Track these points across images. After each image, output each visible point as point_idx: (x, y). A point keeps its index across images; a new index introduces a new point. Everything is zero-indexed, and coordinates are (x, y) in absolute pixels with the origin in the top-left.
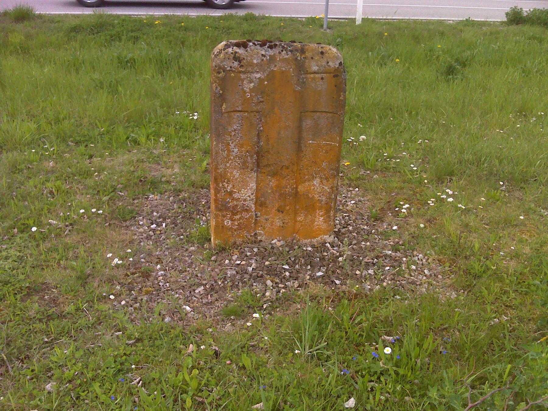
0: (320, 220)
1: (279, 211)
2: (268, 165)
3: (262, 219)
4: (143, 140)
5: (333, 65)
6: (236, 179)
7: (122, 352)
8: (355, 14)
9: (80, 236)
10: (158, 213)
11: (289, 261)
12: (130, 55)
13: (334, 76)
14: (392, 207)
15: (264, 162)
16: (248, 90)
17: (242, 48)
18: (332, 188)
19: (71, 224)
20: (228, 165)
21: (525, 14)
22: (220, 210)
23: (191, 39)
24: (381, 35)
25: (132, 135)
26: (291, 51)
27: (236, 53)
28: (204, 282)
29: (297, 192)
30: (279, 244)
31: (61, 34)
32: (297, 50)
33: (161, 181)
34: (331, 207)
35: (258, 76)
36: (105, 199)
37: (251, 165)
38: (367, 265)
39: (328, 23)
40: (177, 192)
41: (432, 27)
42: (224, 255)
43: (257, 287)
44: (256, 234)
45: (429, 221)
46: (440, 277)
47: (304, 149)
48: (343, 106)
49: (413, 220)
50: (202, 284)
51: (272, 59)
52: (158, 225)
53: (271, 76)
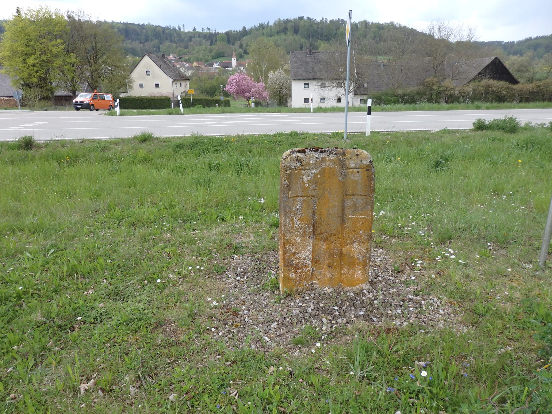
0: (358, 273)
1: (329, 266)
2: (321, 233)
3: (317, 273)
5: (366, 162)
8: (366, 129)
10: (241, 268)
11: (338, 303)
13: (366, 170)
15: (318, 231)
16: (306, 182)
18: (367, 249)
19: (183, 277)
20: (293, 234)
21: (487, 123)
22: (287, 266)
23: (255, 149)
26: (336, 154)
27: (298, 157)
29: (342, 253)
30: (329, 291)
31: (171, 150)
34: (366, 264)
35: (314, 171)
37: (308, 234)
40: (253, 254)
42: (290, 299)
44: (312, 284)
46: (452, 315)
47: (346, 221)
53: (322, 172)
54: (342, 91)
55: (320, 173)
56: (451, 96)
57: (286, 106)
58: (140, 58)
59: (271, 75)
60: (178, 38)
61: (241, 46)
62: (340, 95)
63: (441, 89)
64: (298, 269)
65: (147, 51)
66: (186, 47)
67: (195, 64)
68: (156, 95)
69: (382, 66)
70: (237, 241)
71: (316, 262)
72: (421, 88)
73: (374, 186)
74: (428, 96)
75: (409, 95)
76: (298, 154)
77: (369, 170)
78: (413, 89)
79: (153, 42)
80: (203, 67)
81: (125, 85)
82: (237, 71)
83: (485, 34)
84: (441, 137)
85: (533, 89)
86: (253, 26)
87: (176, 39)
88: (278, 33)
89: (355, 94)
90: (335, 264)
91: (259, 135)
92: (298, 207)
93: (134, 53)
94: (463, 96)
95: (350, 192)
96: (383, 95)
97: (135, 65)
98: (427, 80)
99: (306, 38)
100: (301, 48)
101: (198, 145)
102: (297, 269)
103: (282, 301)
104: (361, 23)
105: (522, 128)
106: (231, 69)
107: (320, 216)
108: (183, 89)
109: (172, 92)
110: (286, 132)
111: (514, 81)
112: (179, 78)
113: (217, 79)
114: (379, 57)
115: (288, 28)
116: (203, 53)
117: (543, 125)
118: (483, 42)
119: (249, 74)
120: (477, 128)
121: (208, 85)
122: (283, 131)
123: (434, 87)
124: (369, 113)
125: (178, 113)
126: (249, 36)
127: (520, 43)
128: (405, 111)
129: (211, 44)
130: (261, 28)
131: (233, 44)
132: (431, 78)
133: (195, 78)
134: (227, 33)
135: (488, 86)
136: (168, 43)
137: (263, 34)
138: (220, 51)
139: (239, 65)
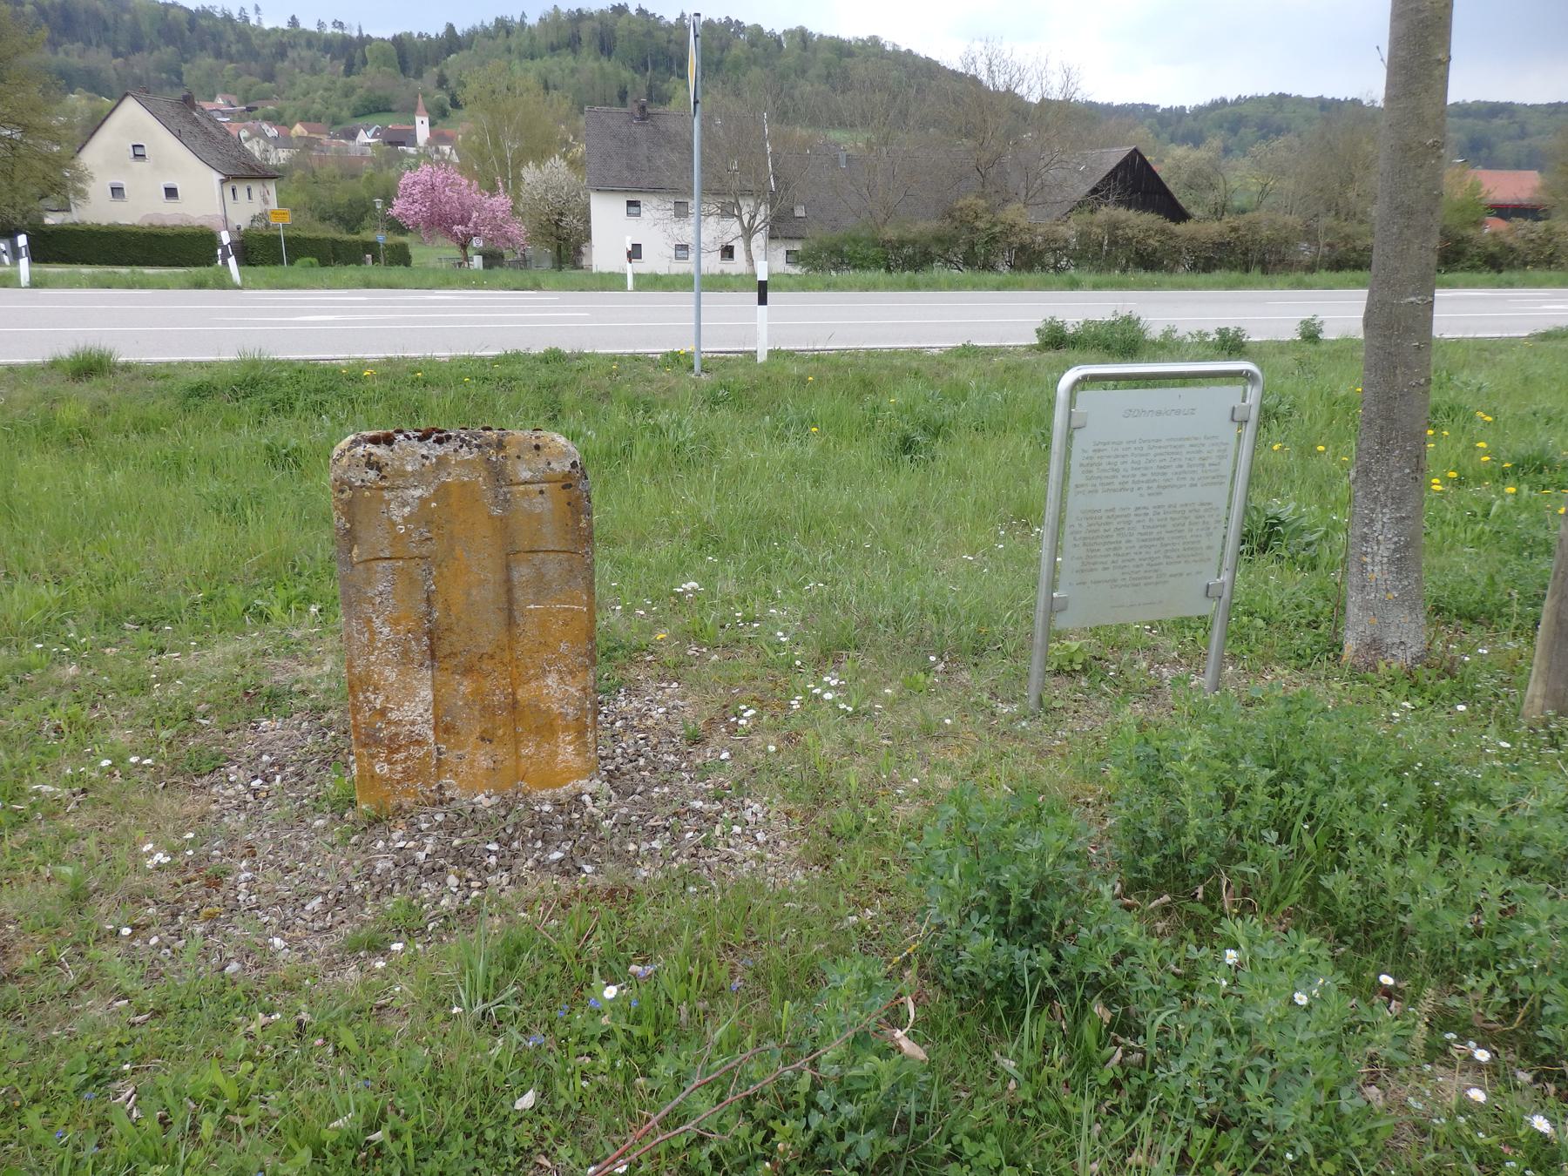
0: (567, 752)
1: (483, 739)
2: (453, 655)
3: (450, 757)
4: (277, 609)
5: (561, 467)
6: (392, 685)
7: (113, 1039)
8: (755, 342)
9: (98, 813)
10: (271, 755)
11: (502, 834)
12: (293, 442)
13: (564, 487)
14: (727, 712)
15: (444, 648)
16: (399, 520)
17: (383, 446)
18: (584, 689)
19: (84, 791)
20: (373, 658)
21: (1071, 330)
22: (365, 745)
23: (434, 402)
24: (802, 380)
25: (258, 602)
26: (479, 446)
27: (371, 454)
28: (324, 888)
29: (515, 703)
30: (487, 803)
31: (170, 401)
32: (489, 445)
33: (290, 692)
34: (586, 727)
35: (418, 493)
36: (164, 734)
37: (418, 657)
38: (654, 832)
39: (704, 362)
40: (318, 711)
41: (897, 362)
42: (376, 832)
43: (428, 888)
44: (440, 787)
45: (788, 738)
46: (783, 843)
47: (520, 620)
48: (589, 539)
49: (759, 739)
50: (319, 893)
51: (442, 461)
52: (266, 781)
53: (443, 492)
54: (734, 227)
55: (436, 497)
56: (1022, 248)
57: (576, 265)
58: (115, 102)
59: (530, 173)
60: (240, 46)
61: (442, 82)
62: (727, 239)
63: (997, 229)
64: (397, 750)
65: (138, 81)
66: (269, 77)
67: (298, 129)
68: (169, 223)
69: (843, 160)
70: (280, 674)
71: (447, 730)
72: (947, 226)
73: (590, 525)
74: (964, 248)
75: (914, 242)
76: (371, 448)
77: (570, 486)
78: (925, 226)
79: (156, 53)
80: (325, 139)
81: (61, 183)
82: (428, 158)
83: (1111, 81)
84: (951, 366)
85: (1221, 235)
86: (478, 24)
87: (234, 49)
88: (553, 49)
89: (772, 237)
90: (500, 732)
91: (452, 359)
92: (381, 588)
93: (94, 84)
94: (1054, 251)
95: (525, 544)
96: (845, 242)
97: (95, 124)
98: (961, 203)
99: (635, 69)
100: (623, 96)
101: (259, 388)
102: (392, 751)
103: (354, 839)
104: (790, 34)
105: (1153, 343)
106: (412, 150)
107: (447, 609)
108: (256, 208)
109: (220, 212)
110: (532, 352)
111: (1177, 213)
112: (243, 174)
113: (370, 179)
114: (836, 135)
115: (585, 36)
116: (322, 97)
117: (1202, 335)
118: (1109, 106)
119: (462, 168)
120: (1047, 344)
121: (341, 195)
122: (522, 349)
123: (980, 224)
124: (763, 300)
125: (223, 283)
126: (465, 53)
127: (1200, 111)
128: (887, 289)
129: (349, 71)
130: (503, 33)
131: (419, 75)
132: (971, 199)
133: (298, 173)
134: (398, 41)
135: (1114, 226)
136: (206, 61)
137: (509, 50)
138: (380, 93)
139: (437, 138)
